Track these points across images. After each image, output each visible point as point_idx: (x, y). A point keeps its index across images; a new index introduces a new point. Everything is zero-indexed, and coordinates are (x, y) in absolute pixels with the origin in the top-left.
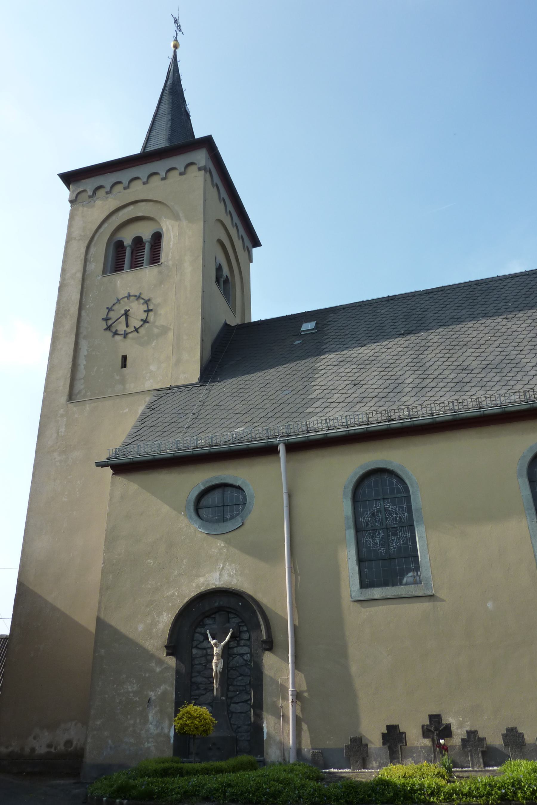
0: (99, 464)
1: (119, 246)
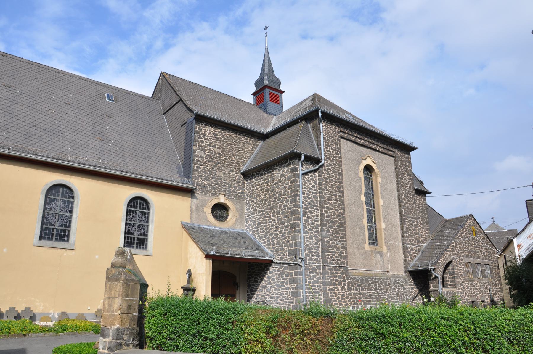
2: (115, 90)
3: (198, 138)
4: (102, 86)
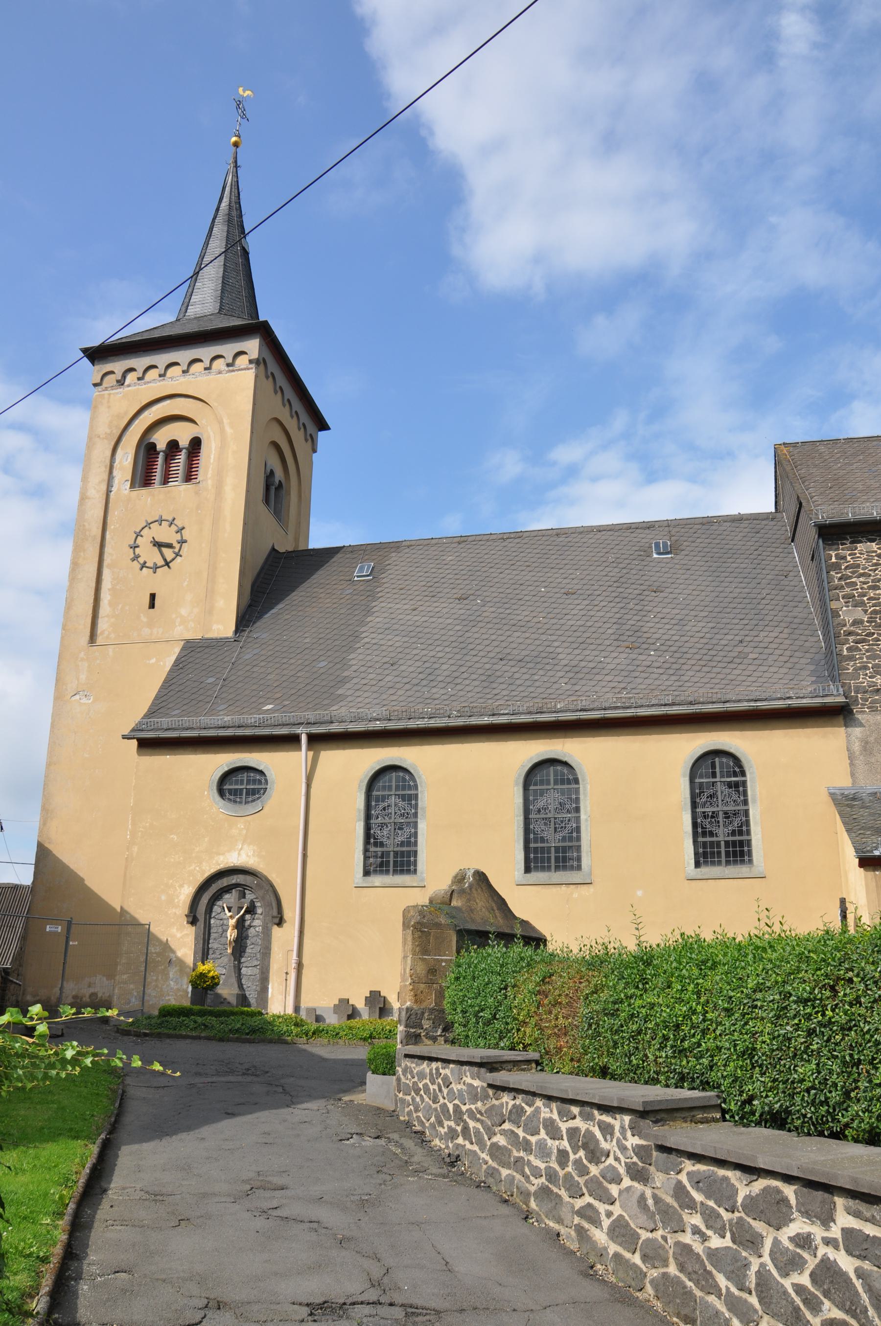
0: (124, 737)
1: (151, 449)
2: (675, 527)
3: (840, 579)
4: (645, 528)
